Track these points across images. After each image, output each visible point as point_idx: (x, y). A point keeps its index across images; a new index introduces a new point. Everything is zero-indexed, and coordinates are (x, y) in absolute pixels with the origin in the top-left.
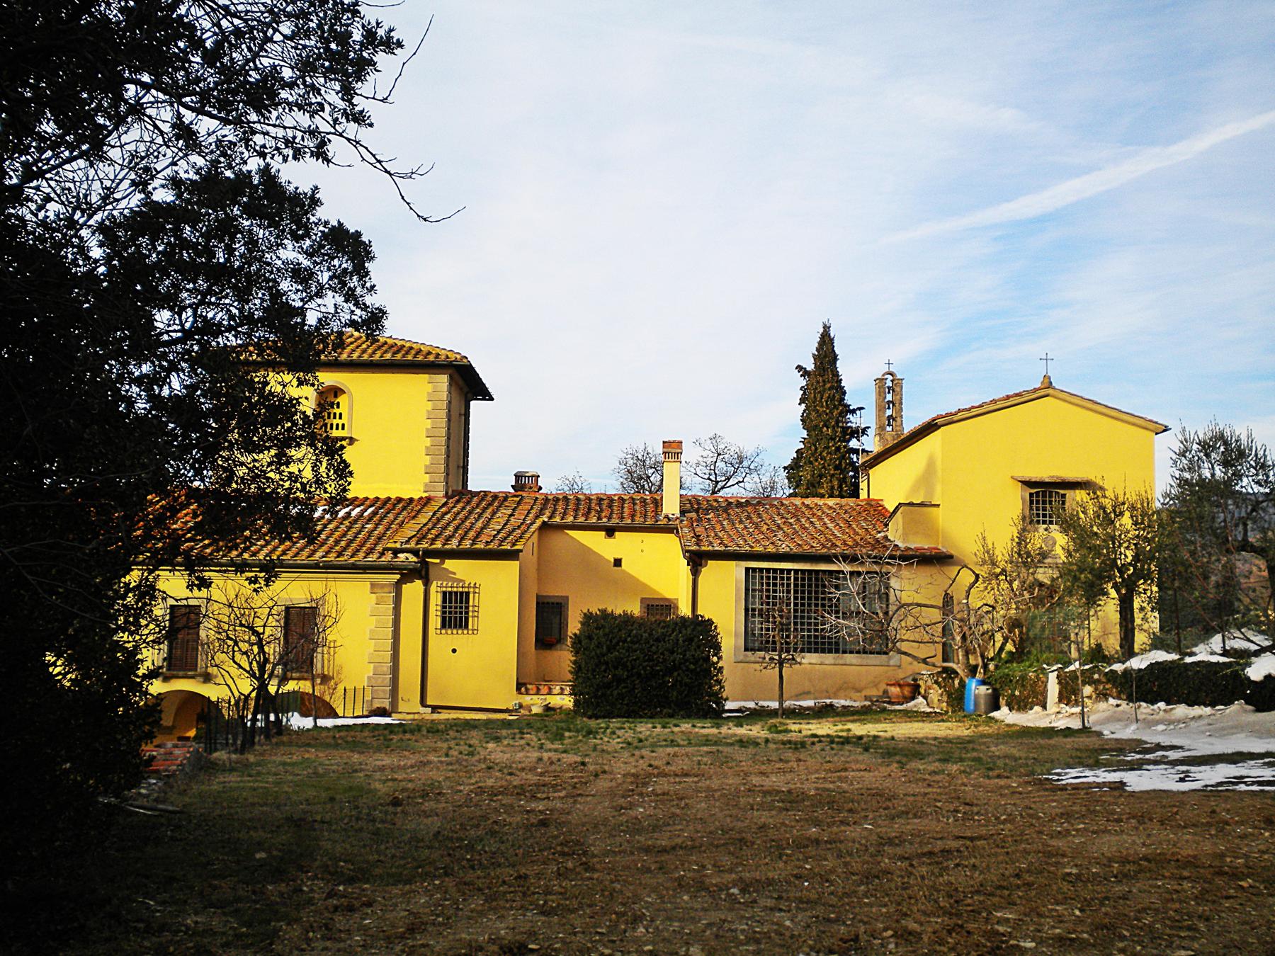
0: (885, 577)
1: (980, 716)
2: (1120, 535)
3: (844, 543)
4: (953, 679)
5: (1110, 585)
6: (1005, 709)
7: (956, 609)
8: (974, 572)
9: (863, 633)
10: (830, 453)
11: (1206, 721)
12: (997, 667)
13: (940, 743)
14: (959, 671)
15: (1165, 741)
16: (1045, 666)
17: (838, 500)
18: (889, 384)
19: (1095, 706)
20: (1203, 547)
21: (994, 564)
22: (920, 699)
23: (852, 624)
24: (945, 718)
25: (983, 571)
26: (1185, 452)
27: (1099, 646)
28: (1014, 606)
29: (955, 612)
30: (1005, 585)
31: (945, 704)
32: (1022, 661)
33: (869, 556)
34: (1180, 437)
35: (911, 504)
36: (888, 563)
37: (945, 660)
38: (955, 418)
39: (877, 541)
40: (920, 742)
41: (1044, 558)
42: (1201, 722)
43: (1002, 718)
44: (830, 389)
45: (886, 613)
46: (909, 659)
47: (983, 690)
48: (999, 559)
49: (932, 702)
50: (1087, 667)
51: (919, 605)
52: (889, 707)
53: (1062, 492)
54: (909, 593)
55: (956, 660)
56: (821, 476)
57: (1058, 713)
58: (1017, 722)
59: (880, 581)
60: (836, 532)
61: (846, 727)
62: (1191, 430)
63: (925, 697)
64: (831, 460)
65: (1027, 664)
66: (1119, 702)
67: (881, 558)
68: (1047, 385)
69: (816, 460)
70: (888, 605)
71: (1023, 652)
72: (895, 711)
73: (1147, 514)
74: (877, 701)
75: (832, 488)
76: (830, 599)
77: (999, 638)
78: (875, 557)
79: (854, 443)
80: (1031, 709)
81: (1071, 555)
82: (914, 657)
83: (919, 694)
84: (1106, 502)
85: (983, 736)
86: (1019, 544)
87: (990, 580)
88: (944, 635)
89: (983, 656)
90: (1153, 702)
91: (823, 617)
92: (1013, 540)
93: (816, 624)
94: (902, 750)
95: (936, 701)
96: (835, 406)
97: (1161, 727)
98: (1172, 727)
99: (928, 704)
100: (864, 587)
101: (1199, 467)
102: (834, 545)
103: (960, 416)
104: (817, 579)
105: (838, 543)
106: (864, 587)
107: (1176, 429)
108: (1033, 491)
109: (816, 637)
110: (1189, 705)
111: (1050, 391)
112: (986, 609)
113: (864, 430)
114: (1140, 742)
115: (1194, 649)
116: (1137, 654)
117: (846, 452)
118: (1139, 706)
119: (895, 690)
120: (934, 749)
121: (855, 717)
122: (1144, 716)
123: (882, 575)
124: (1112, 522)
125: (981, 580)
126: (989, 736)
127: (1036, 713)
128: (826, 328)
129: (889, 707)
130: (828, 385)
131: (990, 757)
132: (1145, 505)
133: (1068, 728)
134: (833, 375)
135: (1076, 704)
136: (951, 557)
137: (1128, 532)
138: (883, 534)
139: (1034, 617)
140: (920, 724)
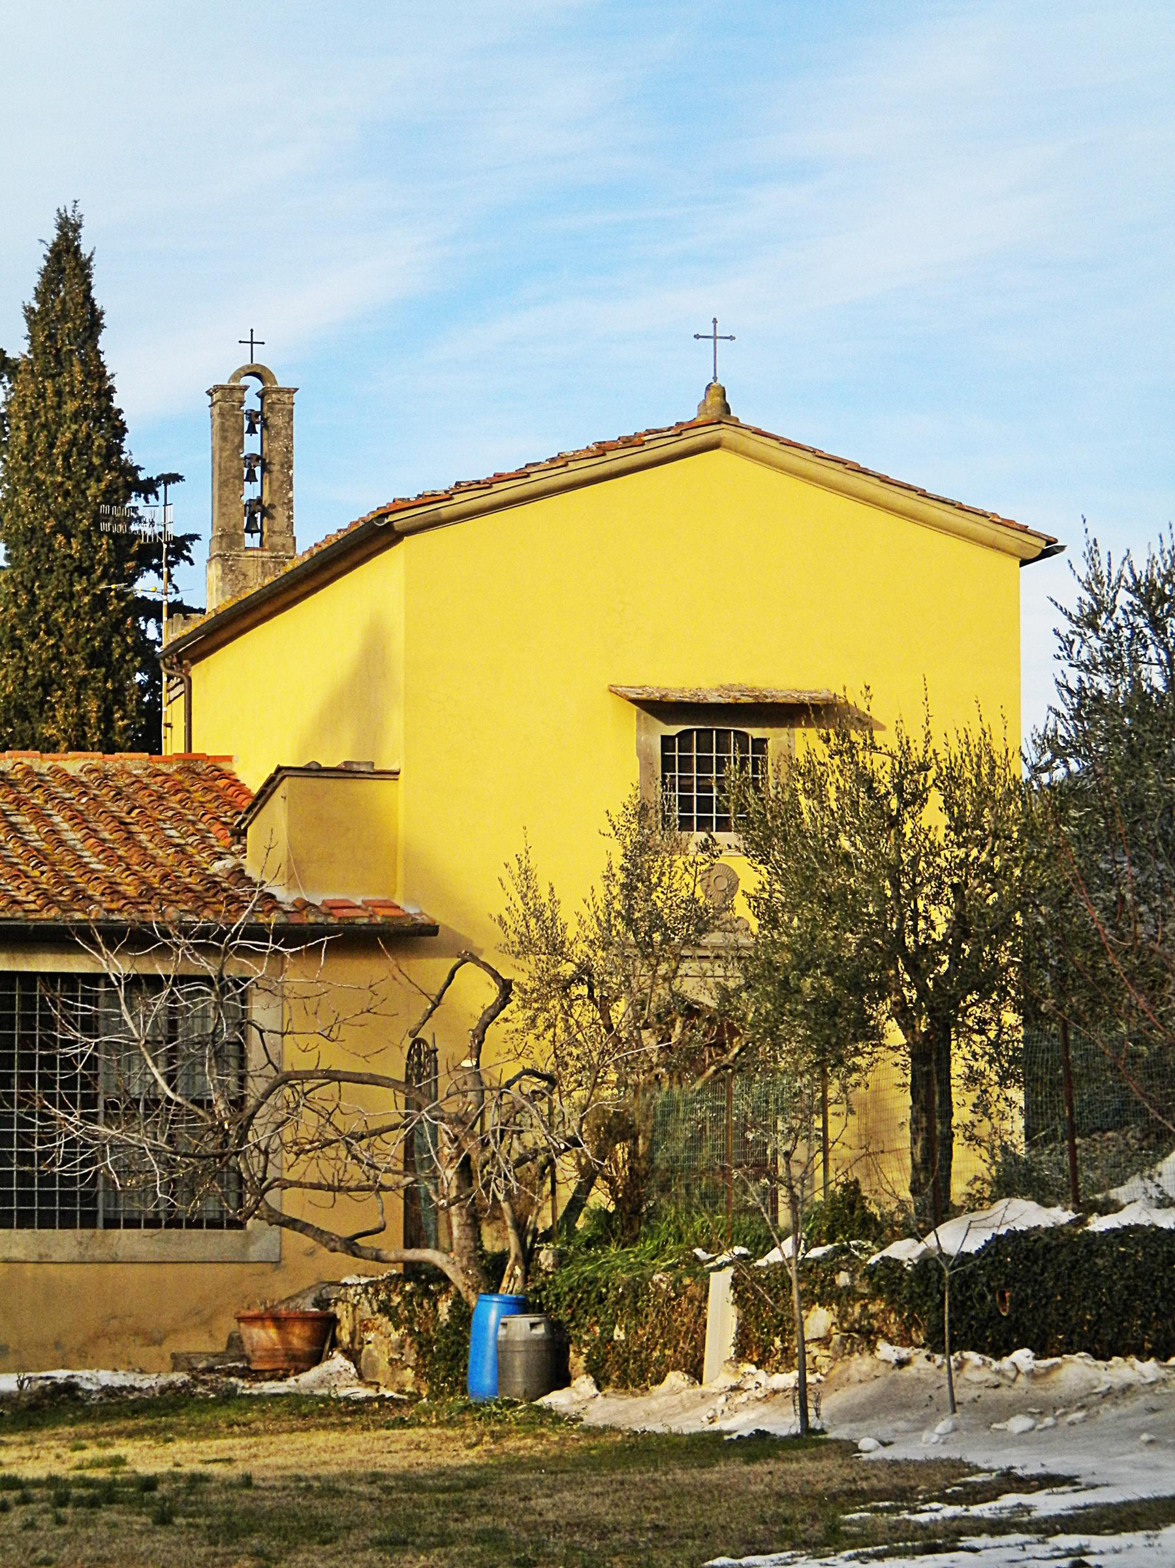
0: (240, 989)
1: (512, 1404)
2: (914, 862)
3: (113, 890)
4: (433, 1297)
5: (886, 1006)
6: (584, 1385)
7: (445, 1084)
8: (496, 975)
9: (169, 1165)
10: (77, 615)
11: (1141, 1402)
12: (561, 1259)
13: (387, 1490)
14: (450, 1272)
15: (1028, 1463)
16: (698, 1251)
17: (95, 759)
18: (252, 403)
19: (839, 1367)
20: (1143, 893)
21: (557, 949)
22: (338, 1362)
23: (134, 1138)
24: (408, 1413)
25: (521, 973)
26: (1096, 614)
27: (852, 1189)
28: (613, 1077)
29: (442, 1095)
30: (585, 1014)
31: (409, 1373)
32: (635, 1240)
33: (185, 931)
34: (1083, 570)
35: (313, 771)
36: (242, 951)
37: (411, 1241)
38: (446, 511)
39: (212, 883)
40: (330, 1490)
41: (700, 932)
42: (1128, 1406)
43: (573, 1410)
44: (75, 416)
45: (238, 1103)
46: (308, 1242)
47: (523, 1327)
48: (570, 934)
49: (373, 1365)
50: (816, 1252)
51: (332, 1076)
52: (243, 1386)
53: (755, 733)
54: (301, 1040)
55: (444, 1242)
56: (46, 685)
57: (735, 1389)
58: (620, 1421)
59: (219, 1004)
60: (88, 857)
61: (111, 1452)
62: (1113, 546)
63: (352, 1355)
64: (77, 634)
65: (650, 1246)
66: (905, 1352)
67: (220, 937)
68: (714, 413)
69: (34, 636)
70: (242, 1079)
71: (636, 1211)
72: (260, 1398)
73: (990, 795)
74: (210, 1370)
75: (82, 720)
76: (68, 1063)
77: (567, 1167)
78: (204, 933)
79: (148, 585)
80: (659, 1380)
81: (774, 922)
82: (319, 1234)
83: (335, 1343)
84: (881, 767)
85: (516, 1465)
86: (629, 889)
87: (547, 998)
88: (409, 1165)
89: (520, 1226)
90: (999, 1351)
91: (44, 1117)
92: (609, 877)
93: (25, 1140)
94: (270, 1515)
95: (383, 1364)
96: (91, 468)
97: (1019, 1423)
98: (1049, 1421)
99: (360, 1376)
100: (173, 1025)
101: (1135, 661)
102: (79, 895)
103: (463, 502)
104: (28, 1002)
105: (94, 890)
106: (173, 1025)
107: (1075, 549)
108: (674, 730)
109: (25, 1179)
110: (1097, 1356)
111: (725, 433)
112: (531, 1085)
113: (180, 547)
114: (959, 1467)
115: (1114, 1193)
116: (956, 1212)
117: (126, 612)
118: (961, 1366)
119: (263, 1336)
120: (366, 1507)
121: (143, 1422)
122: (973, 1393)
123: (220, 983)
124: (895, 822)
125: (516, 999)
126: (536, 1464)
127: (675, 1392)
128: (69, 229)
129: (243, 1386)
130: (70, 406)
131: (532, 1528)
132: (985, 770)
133: (761, 1435)
134: (88, 375)
135: (787, 1361)
136: (432, 930)
137: (935, 851)
138: (229, 862)
139: (670, 1108)
140: (334, 1437)
